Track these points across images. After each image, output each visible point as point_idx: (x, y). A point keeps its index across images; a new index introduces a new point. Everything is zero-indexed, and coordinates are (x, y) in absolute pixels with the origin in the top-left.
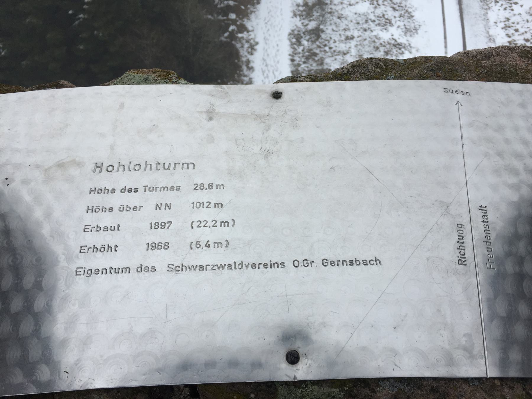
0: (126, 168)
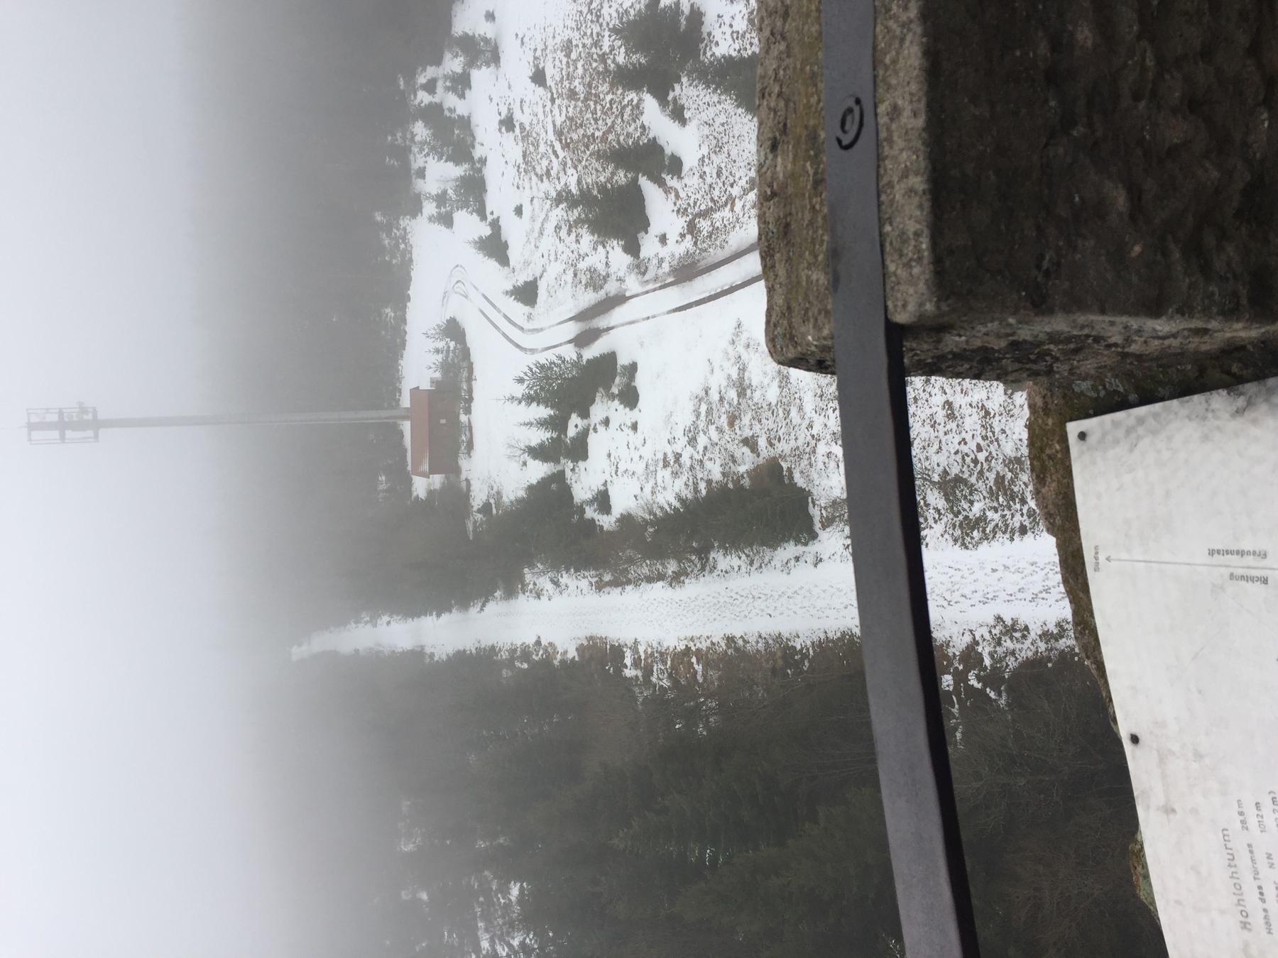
0: (1240, 897)
